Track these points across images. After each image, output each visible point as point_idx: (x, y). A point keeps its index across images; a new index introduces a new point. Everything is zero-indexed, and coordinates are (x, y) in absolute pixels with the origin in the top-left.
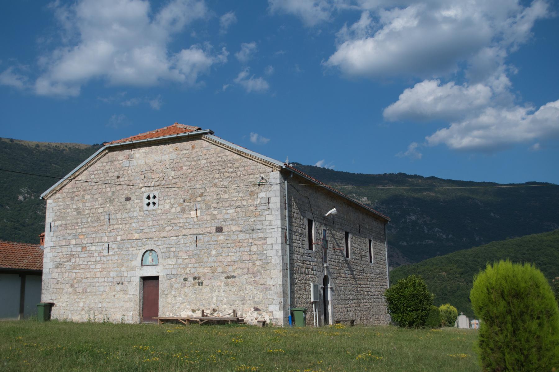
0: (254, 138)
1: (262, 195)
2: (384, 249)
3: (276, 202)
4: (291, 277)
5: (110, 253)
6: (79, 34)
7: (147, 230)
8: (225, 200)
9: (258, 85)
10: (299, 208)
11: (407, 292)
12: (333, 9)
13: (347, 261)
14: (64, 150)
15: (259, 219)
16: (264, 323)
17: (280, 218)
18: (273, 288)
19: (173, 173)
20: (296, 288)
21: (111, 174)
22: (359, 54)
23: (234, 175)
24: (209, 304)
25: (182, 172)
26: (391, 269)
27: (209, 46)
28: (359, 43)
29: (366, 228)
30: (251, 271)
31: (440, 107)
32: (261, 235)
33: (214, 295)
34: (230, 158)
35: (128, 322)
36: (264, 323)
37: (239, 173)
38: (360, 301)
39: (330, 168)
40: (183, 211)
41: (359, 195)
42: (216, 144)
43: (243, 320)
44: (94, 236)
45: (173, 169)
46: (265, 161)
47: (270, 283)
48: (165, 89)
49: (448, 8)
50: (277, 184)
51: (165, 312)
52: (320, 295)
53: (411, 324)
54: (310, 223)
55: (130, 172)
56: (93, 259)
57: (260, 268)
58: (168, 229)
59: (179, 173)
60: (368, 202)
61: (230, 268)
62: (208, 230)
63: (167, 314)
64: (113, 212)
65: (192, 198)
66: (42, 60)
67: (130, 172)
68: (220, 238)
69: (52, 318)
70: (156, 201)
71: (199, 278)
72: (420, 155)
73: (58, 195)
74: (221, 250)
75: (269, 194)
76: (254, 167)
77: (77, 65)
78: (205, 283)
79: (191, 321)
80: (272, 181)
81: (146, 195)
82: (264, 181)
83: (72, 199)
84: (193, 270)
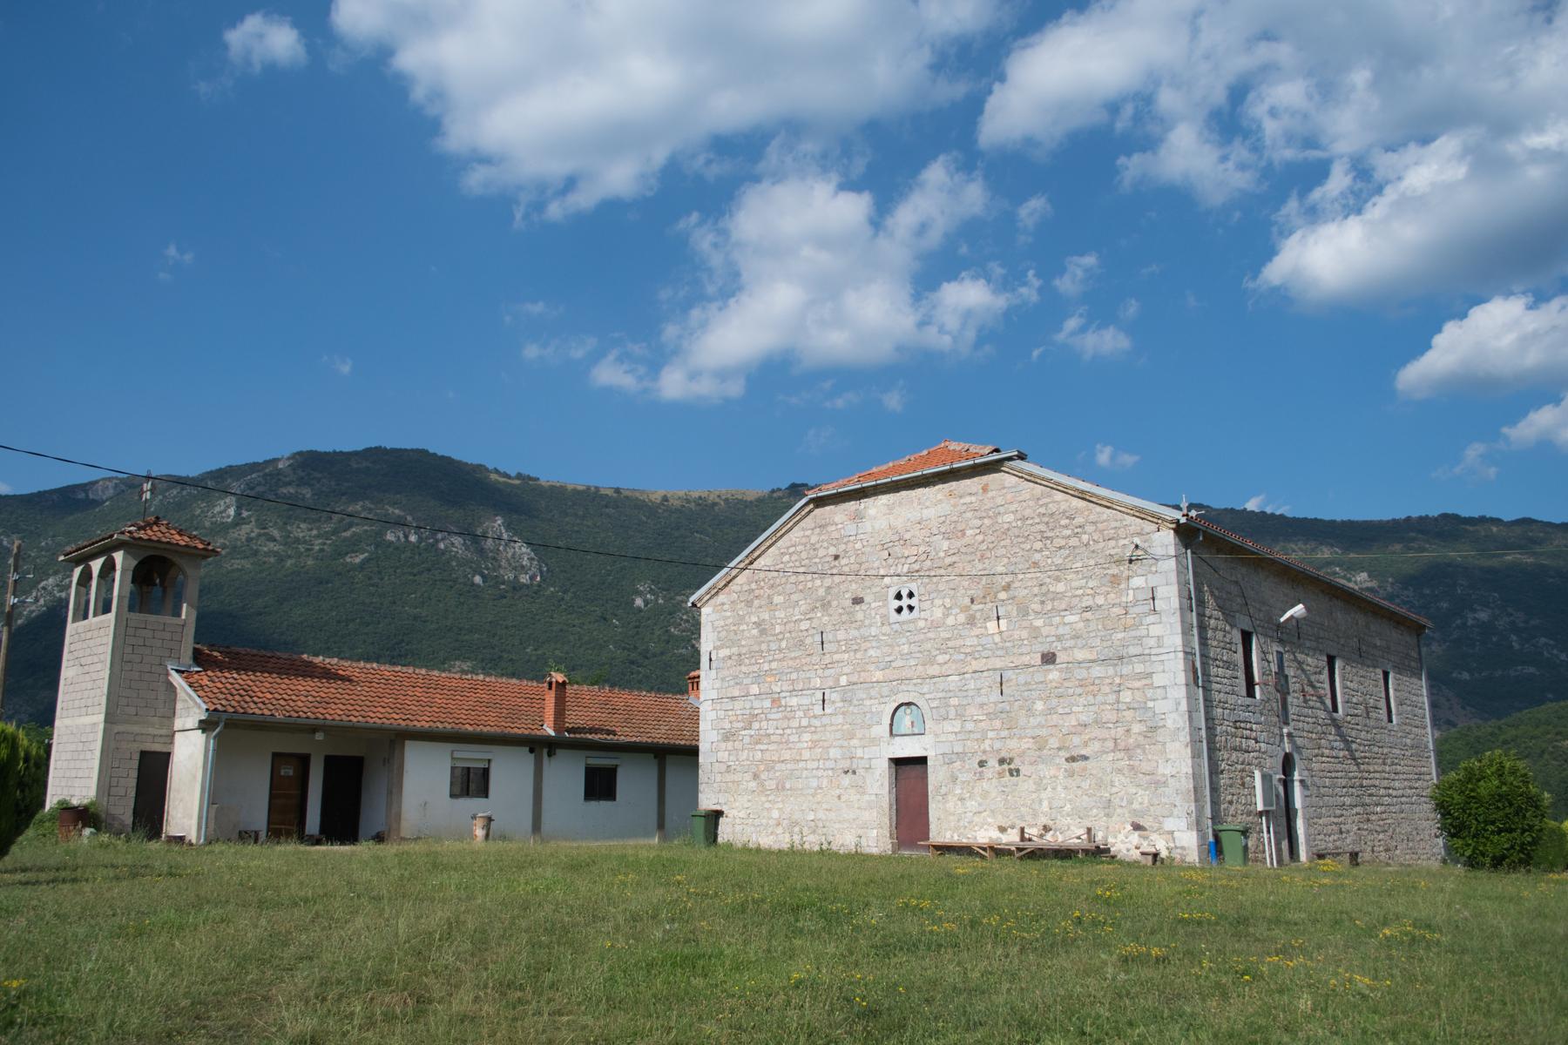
0: (1104, 457)
1: (1137, 582)
2: (1422, 688)
3: (1170, 596)
4: (1210, 758)
5: (827, 711)
6: (737, 275)
7: (899, 663)
8: (1057, 596)
9: (1108, 342)
10: (1221, 608)
11: (1484, 789)
12: (1263, 163)
13: (1333, 720)
14: (715, 504)
15: (1133, 633)
16: (1155, 855)
17: (1179, 630)
18: (1171, 781)
19: (945, 545)
20: (1224, 780)
21: (821, 553)
22: (1329, 255)
23: (1074, 542)
24: (1035, 815)
25: (965, 541)
26: (1437, 734)
27: (998, 270)
28: (1330, 229)
29: (1375, 646)
30: (1122, 745)
31: (1532, 358)
32: (1139, 668)
33: (1044, 795)
34: (1063, 506)
35: (867, 850)
36: (1155, 855)
37: (1085, 538)
38: (1371, 809)
39: (1278, 513)
40: (971, 621)
41: (1349, 569)
42: (1032, 479)
43: (1108, 850)
44: (794, 676)
45: (947, 536)
46: (1141, 510)
47: (1165, 770)
48: (915, 370)
49: (1540, 129)
50: (1170, 557)
51: (943, 829)
52: (1278, 796)
53: (1497, 862)
54: (1246, 638)
55: (858, 546)
56: (795, 724)
57: (1141, 738)
58: (941, 659)
59: (959, 543)
60: (1369, 585)
61: (1076, 740)
62: (1026, 659)
63: (948, 835)
64: (829, 627)
65: (989, 594)
66: (670, 331)
67: (858, 546)
68: (1050, 677)
69: (720, 840)
70: (913, 602)
71: (1011, 760)
72: (1492, 471)
73: (721, 598)
74: (1054, 702)
75: (1153, 580)
76: (1118, 524)
77: (734, 336)
78: (1023, 770)
79: (998, 852)
80: (1158, 551)
81: (892, 592)
82: (1139, 552)
83: (749, 603)
84: (997, 745)
